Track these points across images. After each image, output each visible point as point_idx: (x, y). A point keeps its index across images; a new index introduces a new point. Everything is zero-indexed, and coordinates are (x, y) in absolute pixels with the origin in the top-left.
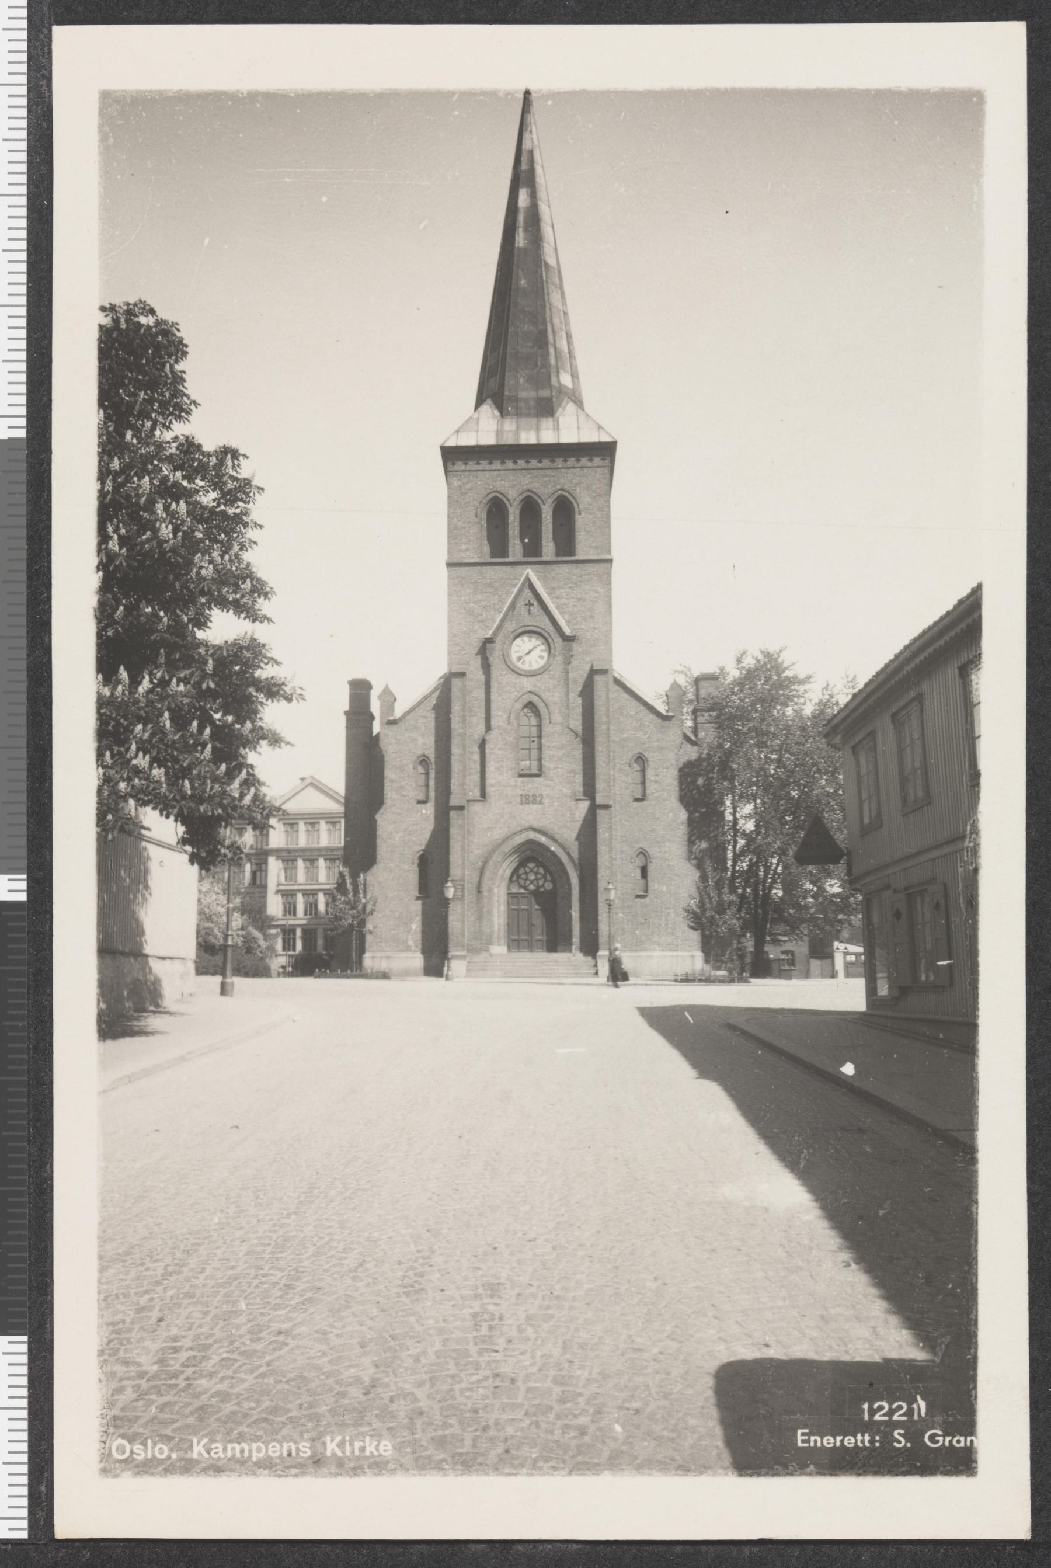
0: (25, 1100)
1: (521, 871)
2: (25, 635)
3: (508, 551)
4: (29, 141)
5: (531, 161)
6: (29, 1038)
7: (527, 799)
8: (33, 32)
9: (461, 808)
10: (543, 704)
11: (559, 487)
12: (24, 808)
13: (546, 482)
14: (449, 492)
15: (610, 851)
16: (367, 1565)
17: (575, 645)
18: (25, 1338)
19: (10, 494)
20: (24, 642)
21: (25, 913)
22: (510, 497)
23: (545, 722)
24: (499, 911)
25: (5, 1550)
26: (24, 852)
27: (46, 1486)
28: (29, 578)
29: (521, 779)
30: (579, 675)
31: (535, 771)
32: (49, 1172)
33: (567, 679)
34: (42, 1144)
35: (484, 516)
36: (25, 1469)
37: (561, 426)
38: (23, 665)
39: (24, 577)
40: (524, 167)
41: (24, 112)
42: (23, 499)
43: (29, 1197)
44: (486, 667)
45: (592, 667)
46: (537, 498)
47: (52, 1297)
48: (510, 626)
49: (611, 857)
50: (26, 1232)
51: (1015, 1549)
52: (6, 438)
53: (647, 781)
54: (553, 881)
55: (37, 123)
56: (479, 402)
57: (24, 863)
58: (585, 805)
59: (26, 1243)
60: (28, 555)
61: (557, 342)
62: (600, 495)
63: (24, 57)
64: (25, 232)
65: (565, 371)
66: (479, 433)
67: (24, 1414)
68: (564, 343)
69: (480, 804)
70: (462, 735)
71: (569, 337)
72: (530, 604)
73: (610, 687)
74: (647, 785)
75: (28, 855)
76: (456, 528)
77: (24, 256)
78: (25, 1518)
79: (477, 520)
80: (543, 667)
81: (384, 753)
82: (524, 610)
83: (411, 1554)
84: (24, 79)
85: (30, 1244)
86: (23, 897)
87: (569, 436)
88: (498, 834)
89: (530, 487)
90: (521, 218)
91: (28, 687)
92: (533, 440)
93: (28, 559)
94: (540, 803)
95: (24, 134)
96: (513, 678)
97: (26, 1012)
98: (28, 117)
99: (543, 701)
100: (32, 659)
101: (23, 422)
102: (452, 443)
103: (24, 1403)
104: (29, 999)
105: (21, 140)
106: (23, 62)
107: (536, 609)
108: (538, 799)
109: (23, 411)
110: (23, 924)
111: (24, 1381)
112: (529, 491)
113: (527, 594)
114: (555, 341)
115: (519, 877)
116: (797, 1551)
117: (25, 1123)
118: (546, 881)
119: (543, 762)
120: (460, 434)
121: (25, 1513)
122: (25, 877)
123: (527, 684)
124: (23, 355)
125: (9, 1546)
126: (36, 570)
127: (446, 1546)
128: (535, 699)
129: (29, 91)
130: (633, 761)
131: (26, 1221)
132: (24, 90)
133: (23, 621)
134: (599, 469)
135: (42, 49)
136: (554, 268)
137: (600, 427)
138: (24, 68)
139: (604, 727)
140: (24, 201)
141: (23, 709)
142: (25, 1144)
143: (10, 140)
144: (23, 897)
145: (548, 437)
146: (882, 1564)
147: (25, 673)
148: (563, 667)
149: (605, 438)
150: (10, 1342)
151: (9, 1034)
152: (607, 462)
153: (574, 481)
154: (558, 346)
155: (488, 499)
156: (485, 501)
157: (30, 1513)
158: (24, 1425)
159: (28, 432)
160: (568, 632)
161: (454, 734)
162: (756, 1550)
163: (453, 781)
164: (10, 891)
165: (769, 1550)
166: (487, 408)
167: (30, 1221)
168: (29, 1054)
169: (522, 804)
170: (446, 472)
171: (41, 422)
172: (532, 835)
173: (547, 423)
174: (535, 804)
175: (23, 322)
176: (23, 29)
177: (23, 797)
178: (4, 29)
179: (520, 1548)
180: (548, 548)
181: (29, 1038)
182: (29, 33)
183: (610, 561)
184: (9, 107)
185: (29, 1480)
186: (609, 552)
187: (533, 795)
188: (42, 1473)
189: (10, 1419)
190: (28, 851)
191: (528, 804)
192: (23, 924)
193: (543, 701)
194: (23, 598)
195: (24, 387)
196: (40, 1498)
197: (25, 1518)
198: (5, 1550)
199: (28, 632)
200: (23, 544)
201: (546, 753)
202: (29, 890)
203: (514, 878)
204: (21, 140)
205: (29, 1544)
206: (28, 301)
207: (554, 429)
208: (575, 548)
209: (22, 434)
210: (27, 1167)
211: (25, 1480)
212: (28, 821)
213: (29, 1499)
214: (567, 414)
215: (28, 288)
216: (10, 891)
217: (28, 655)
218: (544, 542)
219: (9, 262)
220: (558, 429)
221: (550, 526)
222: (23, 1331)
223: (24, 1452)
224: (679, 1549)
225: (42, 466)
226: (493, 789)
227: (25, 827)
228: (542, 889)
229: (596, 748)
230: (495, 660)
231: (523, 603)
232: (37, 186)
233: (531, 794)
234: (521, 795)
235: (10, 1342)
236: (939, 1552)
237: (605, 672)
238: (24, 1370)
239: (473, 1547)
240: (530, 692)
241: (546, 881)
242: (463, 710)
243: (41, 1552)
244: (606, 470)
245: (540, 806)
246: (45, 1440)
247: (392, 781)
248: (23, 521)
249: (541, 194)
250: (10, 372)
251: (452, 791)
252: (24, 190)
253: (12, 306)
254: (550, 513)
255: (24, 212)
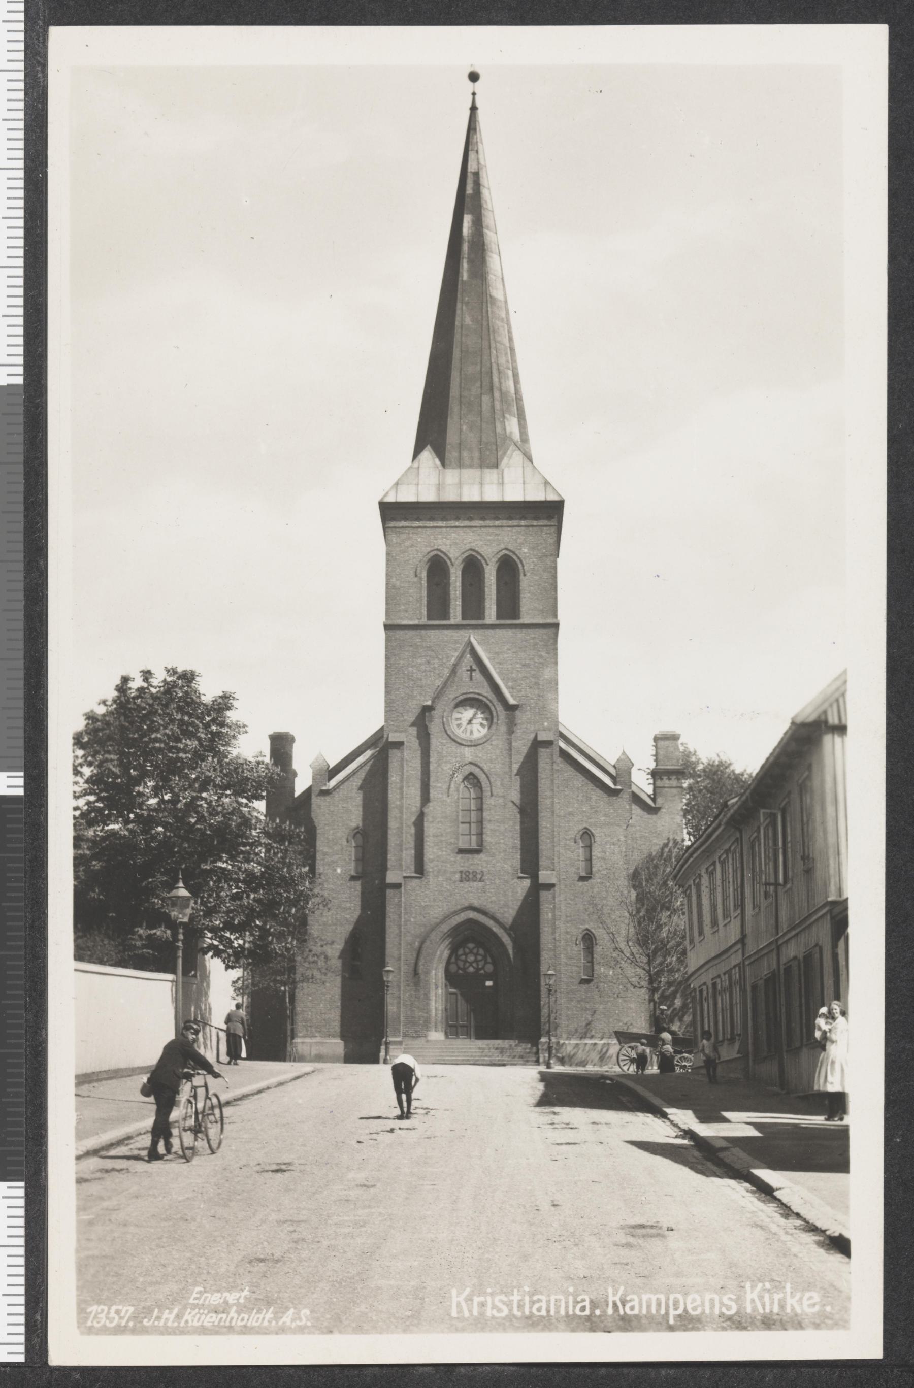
0: (23, 973)
1: (460, 952)
2: (23, 559)
3: (449, 613)
4: (25, 121)
5: (477, 184)
6: (26, 917)
7: (467, 876)
8: (29, 24)
9: (398, 886)
10: (484, 776)
11: (502, 546)
12: (21, 713)
13: (489, 540)
14: (387, 550)
15: (553, 933)
16: (326, 1385)
17: (517, 713)
18: (22, 1184)
19: (8, 434)
20: (21, 566)
21: (23, 806)
22: (451, 556)
23: (487, 793)
24: (436, 994)
25: (5, 1372)
26: (21, 752)
27: (41, 1315)
28: (26, 509)
29: (460, 855)
30: (522, 746)
31: (474, 846)
32: (44, 1036)
33: (510, 749)
34: (38, 1012)
35: (424, 575)
36: (22, 1300)
37: (506, 480)
38: (21, 586)
39: (21, 508)
40: (469, 190)
41: (21, 95)
42: (20, 439)
43: (26, 1059)
44: (424, 737)
45: (536, 736)
46: (479, 558)
47: (46, 1147)
48: (453, 694)
49: (555, 939)
50: (23, 1090)
51: (902, 1372)
52: (5, 384)
53: (594, 858)
54: (494, 963)
55: (33, 105)
56: (418, 450)
57: (21, 762)
58: (527, 883)
59: (23, 1100)
60: (25, 488)
61: (503, 384)
62: (546, 556)
63: (21, 46)
64: (22, 201)
65: (510, 415)
66: (420, 486)
67: (22, 1251)
68: (511, 383)
69: (417, 881)
70: (401, 808)
71: (516, 376)
72: (472, 670)
73: (555, 759)
74: (594, 862)
75: (25, 755)
76: (394, 587)
77: (21, 223)
78: (22, 1344)
79: (416, 579)
80: (485, 736)
81: (316, 824)
82: (465, 676)
83: (365, 1375)
84: (21, 66)
85: (26, 1100)
86: (20, 792)
87: (514, 494)
88: (437, 912)
89: (473, 545)
90: (465, 247)
91: (25, 606)
92: (476, 498)
93: (24, 492)
94: (481, 880)
95: (21, 115)
96: (454, 747)
97: (23, 894)
98: (25, 100)
99: (485, 773)
100: (28, 580)
101: (20, 370)
102: (391, 499)
103: (22, 1241)
104: (26, 882)
105: (18, 120)
106: (21, 51)
107: (477, 675)
108: (479, 876)
109: (21, 360)
110: (20, 816)
111: (22, 1222)
112: (471, 550)
113: (468, 658)
114: (500, 383)
115: (457, 958)
116: (708, 1373)
117: (22, 992)
118: (486, 963)
119: (484, 836)
120: (399, 486)
121: (22, 1339)
122: (22, 774)
123: (468, 754)
124: (21, 311)
125: (8, 1369)
126: (32, 501)
127: (396, 1368)
128: (477, 771)
129: (26, 76)
130: (579, 836)
131: (23, 1080)
132: (21, 76)
133: (21, 547)
134: (545, 528)
135: (37, 39)
136: (500, 301)
137: (547, 483)
138: (21, 56)
139: (548, 802)
140: (21, 174)
141: (21, 625)
142: (23, 1012)
143: (9, 120)
144: (20, 792)
145: (492, 494)
146: (783, 1384)
147: (23, 593)
148: (505, 736)
149: (552, 497)
150: (9, 1188)
151: (8, 914)
152: (554, 522)
153: (519, 541)
154: (504, 389)
155: (429, 557)
156: (426, 559)
157: (27, 1339)
158: (22, 1261)
159: (25, 379)
160: (512, 701)
161: (391, 806)
162: (672, 1372)
163: (389, 856)
164: (8, 787)
165: (684, 1372)
166: (427, 455)
167: (26, 1080)
168: (26, 931)
169: (461, 881)
170: (385, 529)
171: (36, 370)
172: (472, 915)
173: (491, 475)
174: (475, 881)
175: (21, 282)
176: (21, 21)
177: (21, 703)
178: (3, 21)
179: (462, 1370)
180: (491, 613)
181: (26, 917)
182: (26, 25)
183: (556, 626)
184: (8, 90)
185: (26, 1309)
186: (556, 616)
187: (473, 872)
188: (37, 1303)
189: (9, 1256)
190: (25, 751)
191: (468, 881)
192: (20, 816)
193: (485, 773)
194: (21, 527)
195: (22, 339)
196: (35, 1325)
197: (22, 1344)
198: (5, 1372)
199: (25, 557)
200: (21, 478)
201: (488, 827)
202: (26, 786)
203: (453, 960)
204: (18, 120)
205: (25, 1367)
206: (25, 262)
207: (499, 483)
208: (519, 610)
209: (20, 380)
210: (24, 1032)
211: (22, 1310)
212: (25, 725)
213: (26, 1327)
214: (512, 462)
215: (25, 251)
216: (8, 787)
217: (25, 578)
218: (487, 604)
219: (8, 228)
220: (503, 483)
221: (494, 588)
222: (20, 1178)
223: (21, 1285)
224: (603, 1371)
225: (37, 409)
226: (431, 865)
227: (23, 730)
228: (482, 972)
229: (540, 823)
230: (434, 728)
231: (464, 669)
232: (33, 161)
233: (471, 871)
234: (461, 872)
235: (9, 1188)
236: (834, 1373)
237: (549, 744)
238: (22, 1212)
239: (421, 1369)
240: (471, 763)
241: (486, 963)
242: (402, 781)
243: (37, 1374)
244: (553, 529)
245: (481, 884)
246: (40, 1274)
247: (325, 854)
248: (21, 458)
249: (488, 220)
250: (8, 326)
251: (389, 866)
252: (21, 164)
253: (11, 267)
254: (494, 573)
255: (21, 183)
